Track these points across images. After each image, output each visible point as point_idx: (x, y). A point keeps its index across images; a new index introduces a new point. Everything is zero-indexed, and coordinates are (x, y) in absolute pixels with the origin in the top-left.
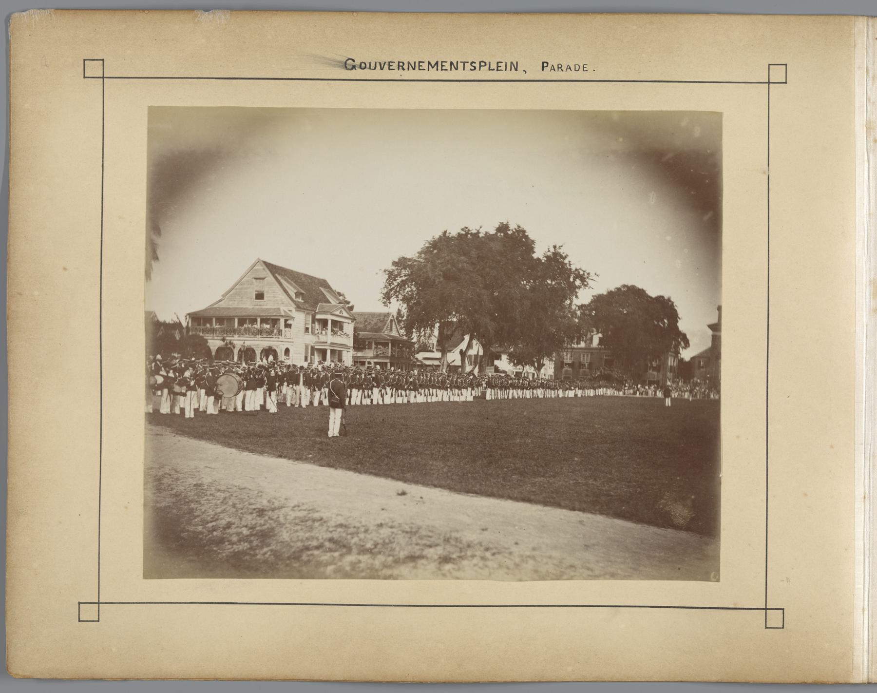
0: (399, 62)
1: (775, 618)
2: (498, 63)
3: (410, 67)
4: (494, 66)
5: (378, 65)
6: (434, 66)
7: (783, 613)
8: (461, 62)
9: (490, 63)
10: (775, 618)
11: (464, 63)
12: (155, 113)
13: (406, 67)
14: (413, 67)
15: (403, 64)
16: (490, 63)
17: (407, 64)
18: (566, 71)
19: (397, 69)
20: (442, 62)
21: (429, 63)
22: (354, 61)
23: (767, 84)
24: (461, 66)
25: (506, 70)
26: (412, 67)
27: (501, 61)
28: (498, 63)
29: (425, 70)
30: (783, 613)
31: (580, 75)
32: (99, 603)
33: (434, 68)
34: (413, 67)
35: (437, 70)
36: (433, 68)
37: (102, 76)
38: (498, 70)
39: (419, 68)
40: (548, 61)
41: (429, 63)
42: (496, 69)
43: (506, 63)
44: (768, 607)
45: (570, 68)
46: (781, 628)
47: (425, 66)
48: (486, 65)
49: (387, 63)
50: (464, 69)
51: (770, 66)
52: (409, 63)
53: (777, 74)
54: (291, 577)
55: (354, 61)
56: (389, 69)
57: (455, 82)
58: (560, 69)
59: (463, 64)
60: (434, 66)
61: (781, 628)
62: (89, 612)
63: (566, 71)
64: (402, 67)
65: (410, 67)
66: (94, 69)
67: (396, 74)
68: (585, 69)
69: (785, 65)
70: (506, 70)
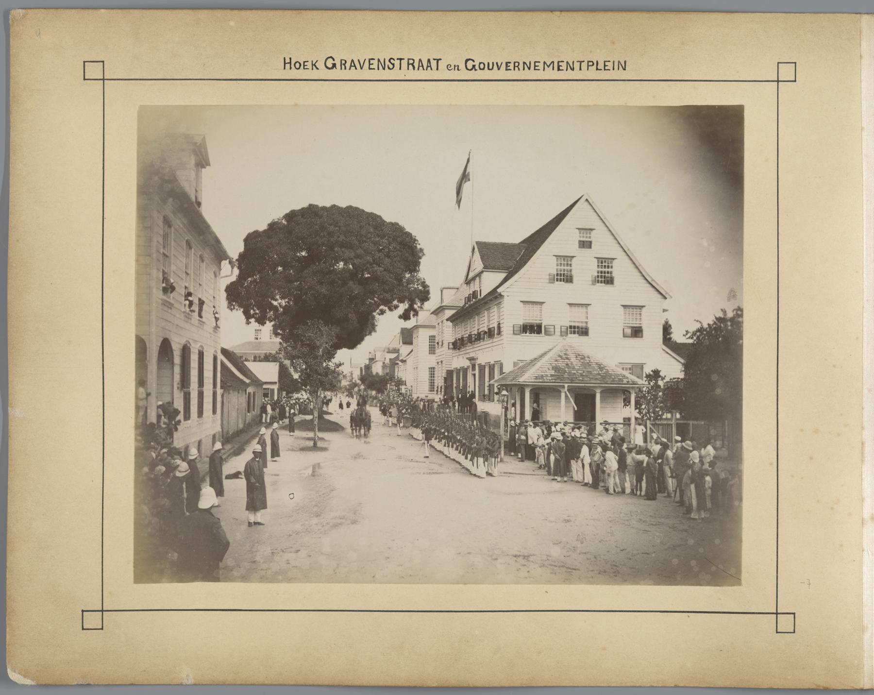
0: (409, 59)
1: (785, 623)
2: (605, 62)
3: (569, 67)
4: (601, 66)
5: (495, 65)
6: (550, 65)
7: (794, 617)
8: (578, 62)
9: (597, 62)
10: (785, 623)
11: (581, 62)
12: (144, 114)
13: (348, 65)
14: (529, 66)
15: (346, 62)
16: (597, 62)
17: (523, 65)
18: (350, 69)
19: (565, 70)
20: (535, 62)
21: (545, 63)
22: (474, 61)
23: (776, 83)
24: (577, 65)
25: (613, 69)
26: (526, 65)
27: (306, 60)
28: (605, 62)
29: (610, 70)
30: (794, 617)
31: (621, 74)
32: (102, 611)
33: (550, 68)
34: (529, 66)
35: (553, 69)
36: (548, 66)
37: (102, 78)
38: (605, 69)
39: (535, 68)
40: (465, 59)
41: (545, 63)
42: (603, 69)
43: (614, 62)
44: (778, 612)
45: (355, 66)
46: (792, 633)
47: (541, 66)
48: (593, 64)
49: (367, 62)
50: (400, 69)
51: (86, 63)
52: (524, 63)
53: (786, 72)
54: (135, 503)
55: (474, 61)
56: (370, 69)
57: (387, 79)
58: (411, 66)
59: (579, 63)
60: (550, 65)
61: (792, 633)
62: (92, 620)
63: (350, 69)
64: (412, 64)
65: (569, 67)
66: (94, 71)
67: (502, 74)
68: (561, 68)
69: (794, 63)
70: (613, 69)
